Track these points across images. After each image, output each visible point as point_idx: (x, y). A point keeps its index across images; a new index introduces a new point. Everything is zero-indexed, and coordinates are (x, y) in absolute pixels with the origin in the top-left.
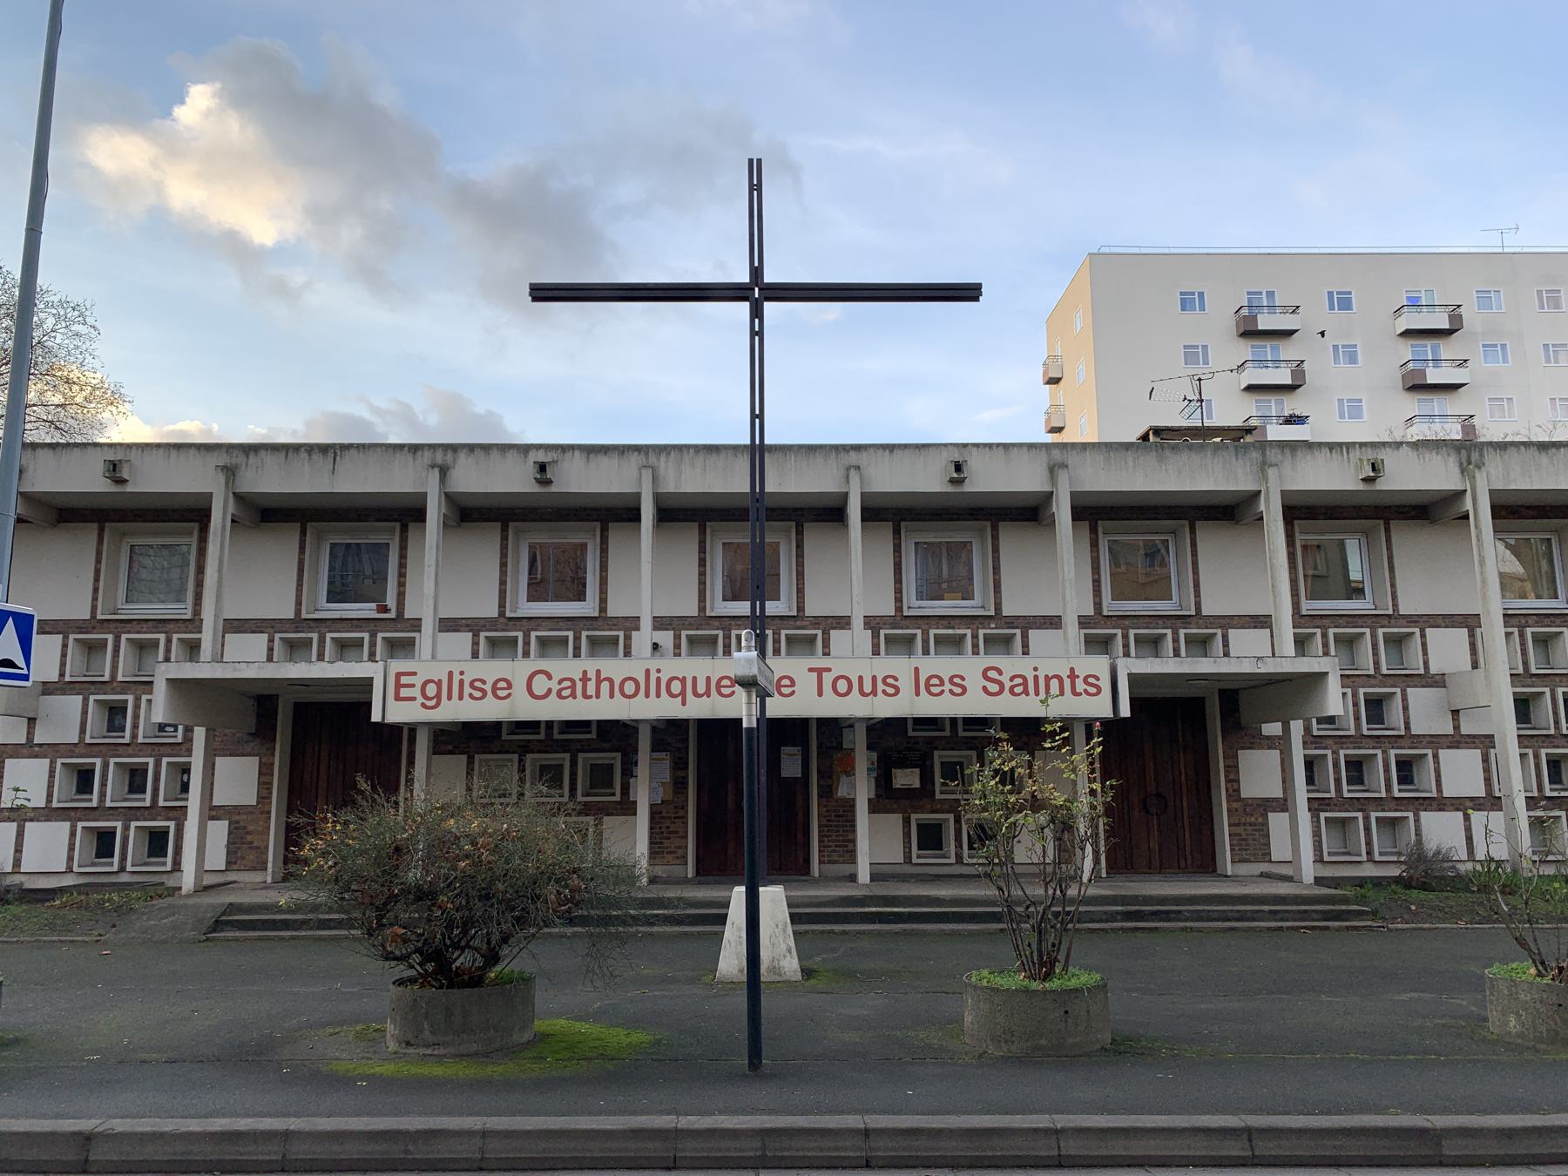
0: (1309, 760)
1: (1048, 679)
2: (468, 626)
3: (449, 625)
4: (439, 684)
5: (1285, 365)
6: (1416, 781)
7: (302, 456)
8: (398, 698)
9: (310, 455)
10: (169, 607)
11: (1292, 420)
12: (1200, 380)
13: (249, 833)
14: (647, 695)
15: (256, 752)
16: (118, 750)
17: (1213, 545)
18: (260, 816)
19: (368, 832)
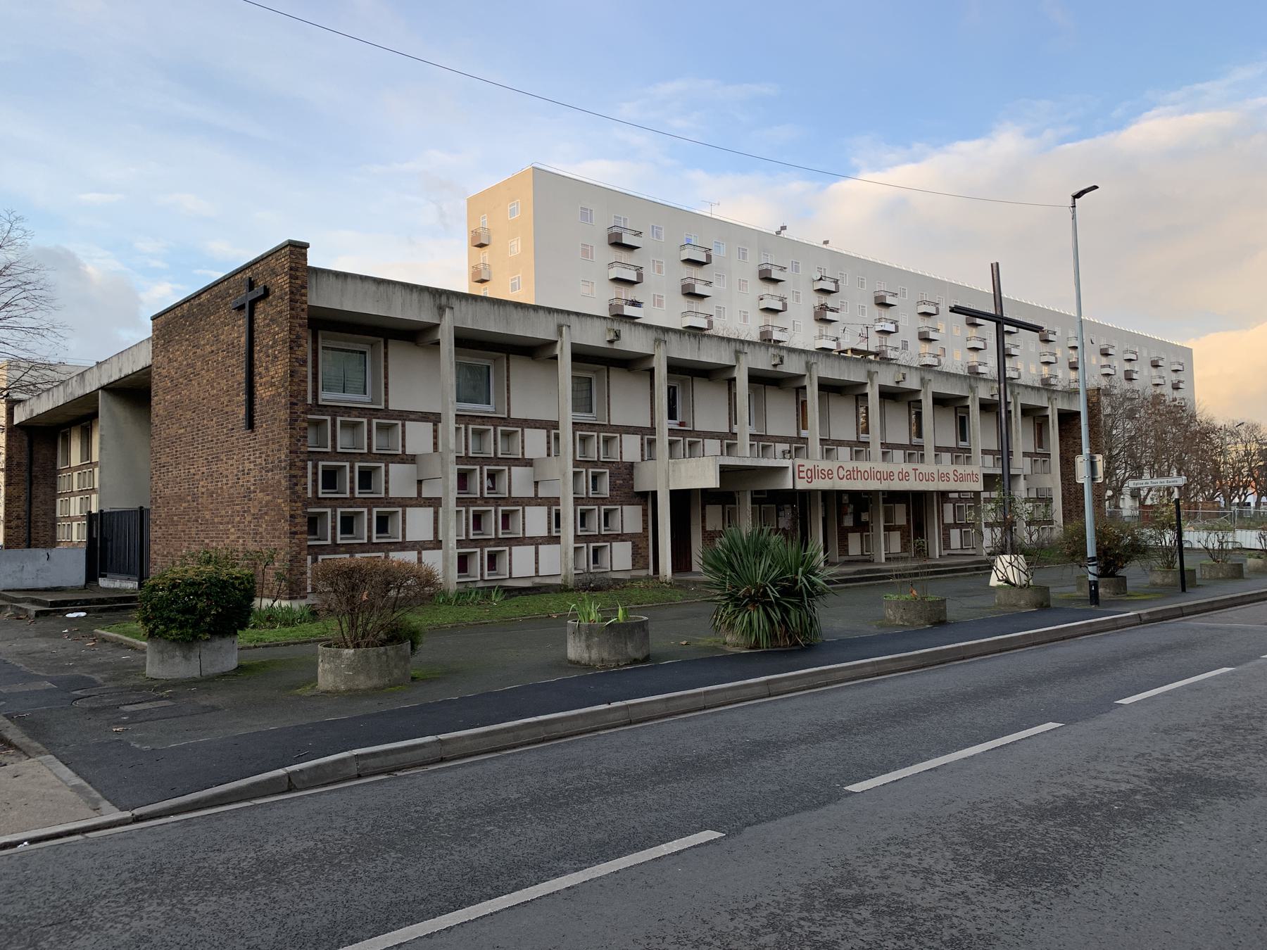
3: (985, 452)
4: (811, 471)
6: (510, 528)
8: (800, 478)
11: (635, 304)
13: (640, 548)
17: (402, 362)
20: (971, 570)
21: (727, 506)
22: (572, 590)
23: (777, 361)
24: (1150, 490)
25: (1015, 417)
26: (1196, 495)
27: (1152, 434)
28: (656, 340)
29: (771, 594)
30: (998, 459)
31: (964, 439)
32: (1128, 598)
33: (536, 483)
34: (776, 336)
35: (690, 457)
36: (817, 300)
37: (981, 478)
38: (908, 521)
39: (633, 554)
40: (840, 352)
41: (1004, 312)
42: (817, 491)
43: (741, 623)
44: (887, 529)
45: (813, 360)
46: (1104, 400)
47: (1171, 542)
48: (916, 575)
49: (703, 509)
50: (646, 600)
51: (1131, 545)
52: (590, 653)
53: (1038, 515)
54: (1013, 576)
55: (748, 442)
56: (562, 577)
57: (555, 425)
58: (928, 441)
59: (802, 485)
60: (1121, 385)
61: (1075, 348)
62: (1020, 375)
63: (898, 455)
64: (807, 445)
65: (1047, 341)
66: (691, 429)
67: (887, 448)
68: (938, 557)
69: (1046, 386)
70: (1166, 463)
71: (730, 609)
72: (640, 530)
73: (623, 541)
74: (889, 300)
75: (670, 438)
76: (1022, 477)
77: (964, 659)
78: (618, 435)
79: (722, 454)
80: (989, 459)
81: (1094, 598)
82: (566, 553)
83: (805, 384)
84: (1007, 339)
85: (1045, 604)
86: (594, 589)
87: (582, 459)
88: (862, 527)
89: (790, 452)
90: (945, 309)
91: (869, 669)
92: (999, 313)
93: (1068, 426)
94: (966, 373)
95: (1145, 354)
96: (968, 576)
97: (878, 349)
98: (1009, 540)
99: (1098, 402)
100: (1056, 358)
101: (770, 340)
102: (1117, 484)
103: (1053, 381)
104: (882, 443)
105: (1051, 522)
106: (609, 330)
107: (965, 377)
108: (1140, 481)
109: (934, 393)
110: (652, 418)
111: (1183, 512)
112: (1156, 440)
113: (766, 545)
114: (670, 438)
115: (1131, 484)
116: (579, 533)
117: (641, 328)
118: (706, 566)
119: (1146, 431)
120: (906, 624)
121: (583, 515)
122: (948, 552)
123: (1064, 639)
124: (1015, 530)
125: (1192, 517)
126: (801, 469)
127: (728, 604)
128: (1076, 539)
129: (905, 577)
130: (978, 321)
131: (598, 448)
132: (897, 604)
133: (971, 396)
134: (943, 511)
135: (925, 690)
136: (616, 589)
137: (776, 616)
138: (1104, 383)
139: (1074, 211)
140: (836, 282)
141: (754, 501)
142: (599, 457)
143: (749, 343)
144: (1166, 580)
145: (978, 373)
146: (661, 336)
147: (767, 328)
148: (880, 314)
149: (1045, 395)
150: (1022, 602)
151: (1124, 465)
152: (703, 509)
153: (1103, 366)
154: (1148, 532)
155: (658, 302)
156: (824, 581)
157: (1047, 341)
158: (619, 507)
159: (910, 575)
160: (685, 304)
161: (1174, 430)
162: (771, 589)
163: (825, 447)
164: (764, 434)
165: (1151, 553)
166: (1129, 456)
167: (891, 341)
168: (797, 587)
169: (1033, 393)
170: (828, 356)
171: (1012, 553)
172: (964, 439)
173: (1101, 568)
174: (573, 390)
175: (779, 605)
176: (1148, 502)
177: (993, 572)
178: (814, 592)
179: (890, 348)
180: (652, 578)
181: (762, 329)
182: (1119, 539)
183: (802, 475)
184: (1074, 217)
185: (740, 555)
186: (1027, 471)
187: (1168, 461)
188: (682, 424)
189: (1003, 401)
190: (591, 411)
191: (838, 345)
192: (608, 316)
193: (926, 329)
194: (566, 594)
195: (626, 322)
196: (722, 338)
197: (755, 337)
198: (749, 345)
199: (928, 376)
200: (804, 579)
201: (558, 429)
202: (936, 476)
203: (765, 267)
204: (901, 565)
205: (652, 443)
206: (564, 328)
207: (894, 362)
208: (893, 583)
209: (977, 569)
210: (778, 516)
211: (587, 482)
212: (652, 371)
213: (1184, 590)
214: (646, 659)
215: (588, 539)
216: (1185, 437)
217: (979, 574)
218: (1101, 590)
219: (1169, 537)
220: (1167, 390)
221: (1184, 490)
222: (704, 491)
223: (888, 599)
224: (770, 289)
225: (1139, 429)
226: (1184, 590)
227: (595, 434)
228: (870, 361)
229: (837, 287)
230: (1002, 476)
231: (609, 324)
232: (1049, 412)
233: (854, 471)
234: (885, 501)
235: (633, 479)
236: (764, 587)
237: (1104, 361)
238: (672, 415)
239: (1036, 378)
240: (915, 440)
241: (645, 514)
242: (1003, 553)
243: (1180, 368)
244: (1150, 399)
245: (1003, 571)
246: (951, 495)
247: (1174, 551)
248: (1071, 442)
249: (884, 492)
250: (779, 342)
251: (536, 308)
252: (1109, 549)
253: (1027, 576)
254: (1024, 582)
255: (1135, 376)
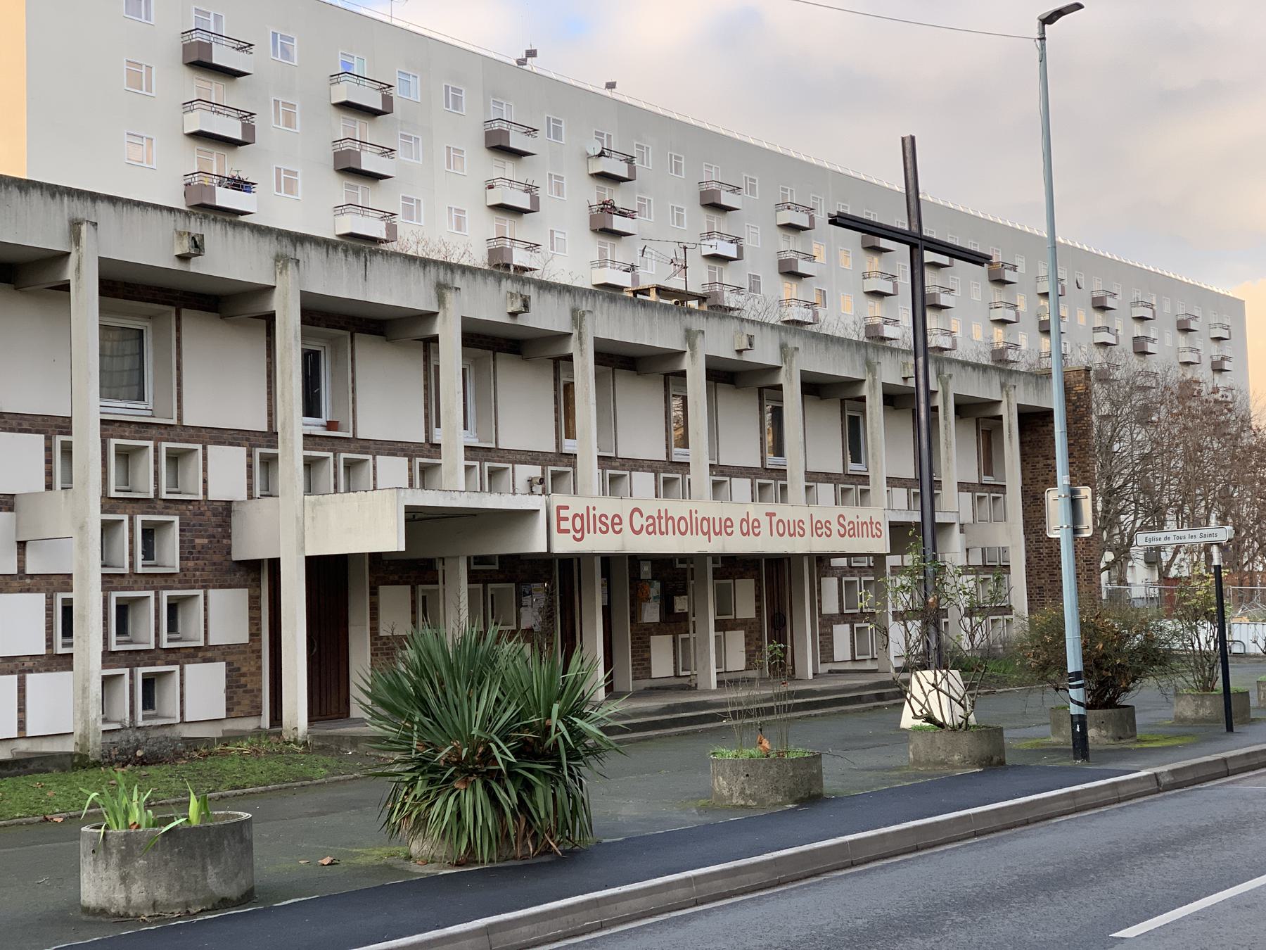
0: (122, 603)
1: (862, 524)
2: (402, 450)
3: (893, 482)
4: (582, 517)
5: (236, 115)
6: (180, 629)
7: (340, 254)
8: (560, 531)
9: (346, 256)
10: (128, 406)
11: (239, 185)
12: (685, 248)
13: (244, 675)
14: (692, 534)
15: (243, 583)
16: (112, 582)
18: (251, 655)
19: (403, 669)
20: (869, 699)
21: (421, 587)
22: (97, 764)
23: (517, 306)
24: (1176, 552)
25: (945, 418)
26: (1251, 560)
27: (1180, 450)
28: (278, 258)
29: (498, 756)
30: (915, 494)
31: (856, 459)
32: (1138, 746)
33: (22, 545)
34: (519, 258)
35: (348, 490)
36: (594, 194)
37: (886, 530)
38: (759, 610)
39: (228, 687)
40: (635, 293)
41: (924, 228)
42: (591, 556)
43: (441, 815)
44: (721, 626)
45: (585, 306)
46: (1098, 390)
47: (1208, 642)
48: (770, 711)
49: (374, 592)
50: (254, 778)
51: (1141, 648)
52: (128, 889)
53: (983, 597)
54: (945, 711)
55: (462, 463)
56: (76, 738)
57: (64, 425)
58: (794, 462)
59: (564, 545)
60: (1128, 365)
61: (1046, 295)
62: (954, 342)
63: (742, 486)
64: (575, 467)
65: (1001, 282)
66: (350, 435)
67: (722, 474)
68: (810, 676)
69: (1000, 364)
70: (1203, 503)
71: (419, 790)
72: (245, 639)
73: (205, 660)
74: (726, 199)
75: (308, 453)
76: (957, 528)
77: (853, 865)
78: (199, 447)
79: (411, 485)
80: (901, 495)
81: (1080, 746)
82: (85, 690)
83: (570, 352)
84: (931, 278)
85: (996, 759)
86: (143, 762)
87: (121, 495)
88: (674, 623)
89: (542, 481)
90: (821, 218)
91: (680, 893)
92: (915, 229)
93: (1034, 437)
94: (862, 337)
95: (1167, 309)
96: (864, 710)
97: (707, 289)
98: (933, 645)
99: (1087, 393)
100: (1017, 314)
101: (507, 266)
102: (1122, 540)
103: (1011, 355)
104: (711, 465)
105: (1008, 610)
106: (181, 235)
107: (858, 344)
108: (1162, 535)
109: (804, 374)
110: (271, 414)
111: (1229, 589)
112: (1186, 462)
113: (490, 661)
114: (308, 453)
115: (1143, 540)
116: (114, 648)
117: (247, 232)
118: (379, 709)
119: (1169, 446)
120: (751, 803)
121: (123, 609)
122: (830, 666)
123: (1027, 823)
124: (946, 623)
125: (1244, 599)
126: (563, 513)
127: (415, 779)
128: (1049, 639)
129: (749, 716)
130: (884, 243)
131: (156, 473)
132: (734, 764)
133: (868, 379)
134: (820, 590)
135: (781, 929)
136: (191, 759)
137: (508, 799)
138: (1098, 359)
139: (1043, 47)
140: (630, 160)
141: (473, 577)
142: (157, 491)
143: (464, 269)
144: (1201, 712)
145: (883, 339)
146: (288, 250)
147: (500, 243)
148: (710, 224)
149: (996, 380)
150: (956, 758)
151: (1133, 506)
152: (374, 592)
153: (1097, 330)
154: (1169, 625)
155: (287, 183)
156: (601, 729)
157: (1001, 282)
158: (201, 592)
159: (759, 712)
160: (340, 189)
161: (1216, 445)
162: (498, 747)
163: (609, 472)
164: (493, 446)
165: (1175, 663)
166: (1141, 490)
167: (729, 275)
168: (550, 741)
169: (975, 376)
170: (613, 299)
171: (938, 667)
172: (856, 459)
173: (1093, 692)
174: (102, 355)
175: (513, 775)
176: (1173, 572)
177: (906, 702)
178: (580, 749)
179: (728, 289)
180: (268, 734)
181: (493, 245)
182: (1122, 638)
183: (564, 525)
184: (1043, 58)
185: (441, 683)
186: (967, 517)
187: (1205, 499)
188: (331, 425)
189: (922, 389)
190: (141, 398)
191: (635, 279)
192: (183, 207)
193: (791, 256)
194: (82, 774)
195: (215, 220)
196: (412, 259)
197: (478, 258)
198: (464, 273)
199: (793, 342)
200: (562, 727)
201: (70, 433)
202: (807, 527)
203: (496, 126)
204: (741, 694)
205: (269, 462)
206: (84, 228)
207: (736, 313)
208: (729, 727)
209: (880, 697)
210: (519, 605)
211: (131, 542)
212: (270, 319)
213: (1230, 728)
214: (247, 897)
215: (133, 658)
216: (1234, 457)
217: (883, 707)
218: (1092, 733)
219: (1205, 634)
220: (1204, 373)
221: (1232, 550)
222: (376, 558)
223: (718, 757)
224: (507, 168)
225: (1156, 442)
226: (1230, 728)
227: (151, 444)
228: (691, 312)
229: (632, 170)
230: (920, 527)
231: (181, 224)
232: (1003, 410)
233: (660, 517)
234: (717, 574)
235: (229, 536)
236: (487, 742)
237: (1099, 319)
238: (311, 407)
239: (982, 349)
240: (771, 460)
241: (254, 605)
242: (924, 667)
243: (1224, 334)
244: (1176, 388)
245: (923, 700)
246: (835, 562)
247: (1212, 659)
248: (1041, 465)
249: (715, 557)
250: (524, 269)
251: (25, 186)
252: (1105, 656)
253: (964, 707)
254: (961, 720)
255: (1150, 347)
